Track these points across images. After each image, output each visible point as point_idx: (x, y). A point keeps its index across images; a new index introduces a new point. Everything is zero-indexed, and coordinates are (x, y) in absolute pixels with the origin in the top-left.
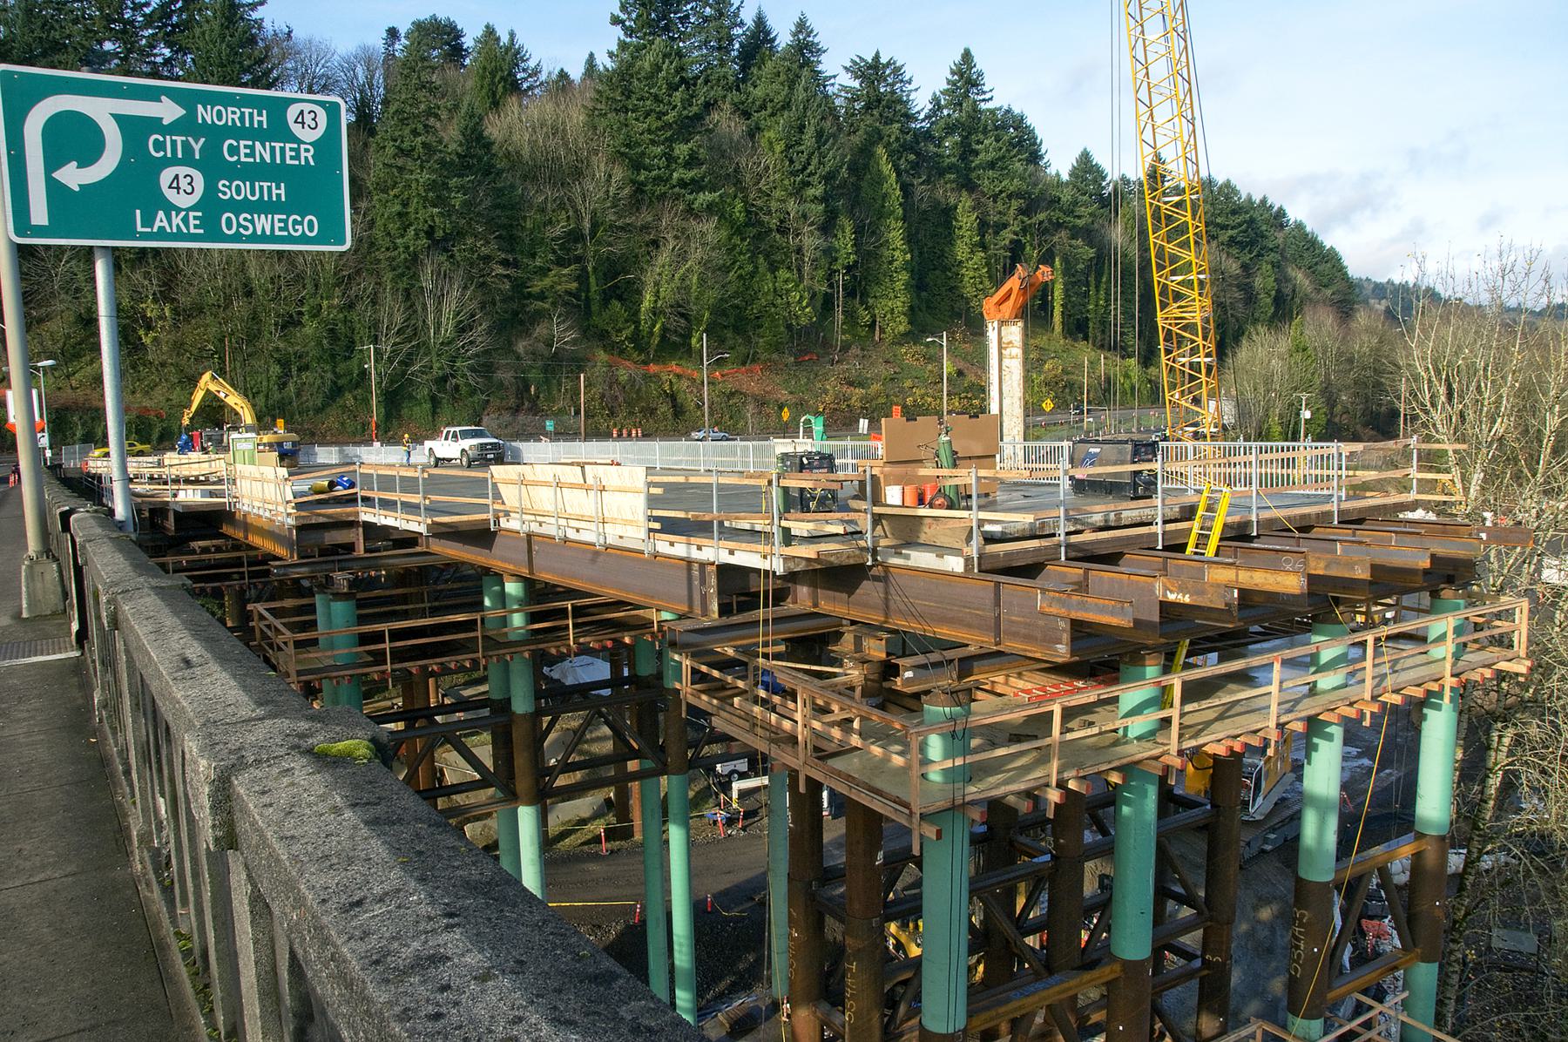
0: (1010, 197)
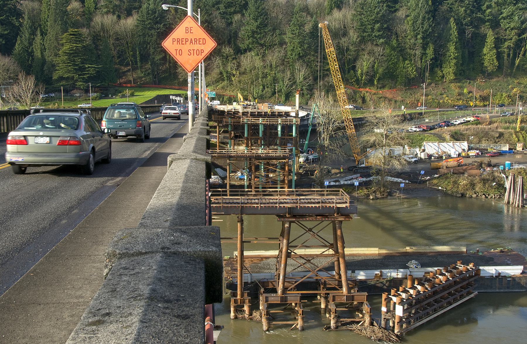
0: (512, 29)
